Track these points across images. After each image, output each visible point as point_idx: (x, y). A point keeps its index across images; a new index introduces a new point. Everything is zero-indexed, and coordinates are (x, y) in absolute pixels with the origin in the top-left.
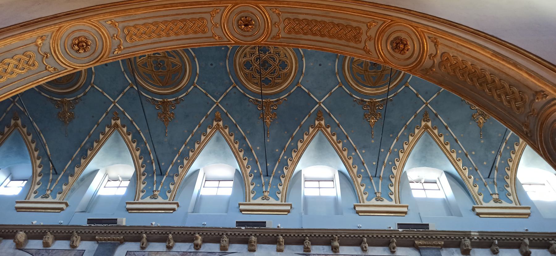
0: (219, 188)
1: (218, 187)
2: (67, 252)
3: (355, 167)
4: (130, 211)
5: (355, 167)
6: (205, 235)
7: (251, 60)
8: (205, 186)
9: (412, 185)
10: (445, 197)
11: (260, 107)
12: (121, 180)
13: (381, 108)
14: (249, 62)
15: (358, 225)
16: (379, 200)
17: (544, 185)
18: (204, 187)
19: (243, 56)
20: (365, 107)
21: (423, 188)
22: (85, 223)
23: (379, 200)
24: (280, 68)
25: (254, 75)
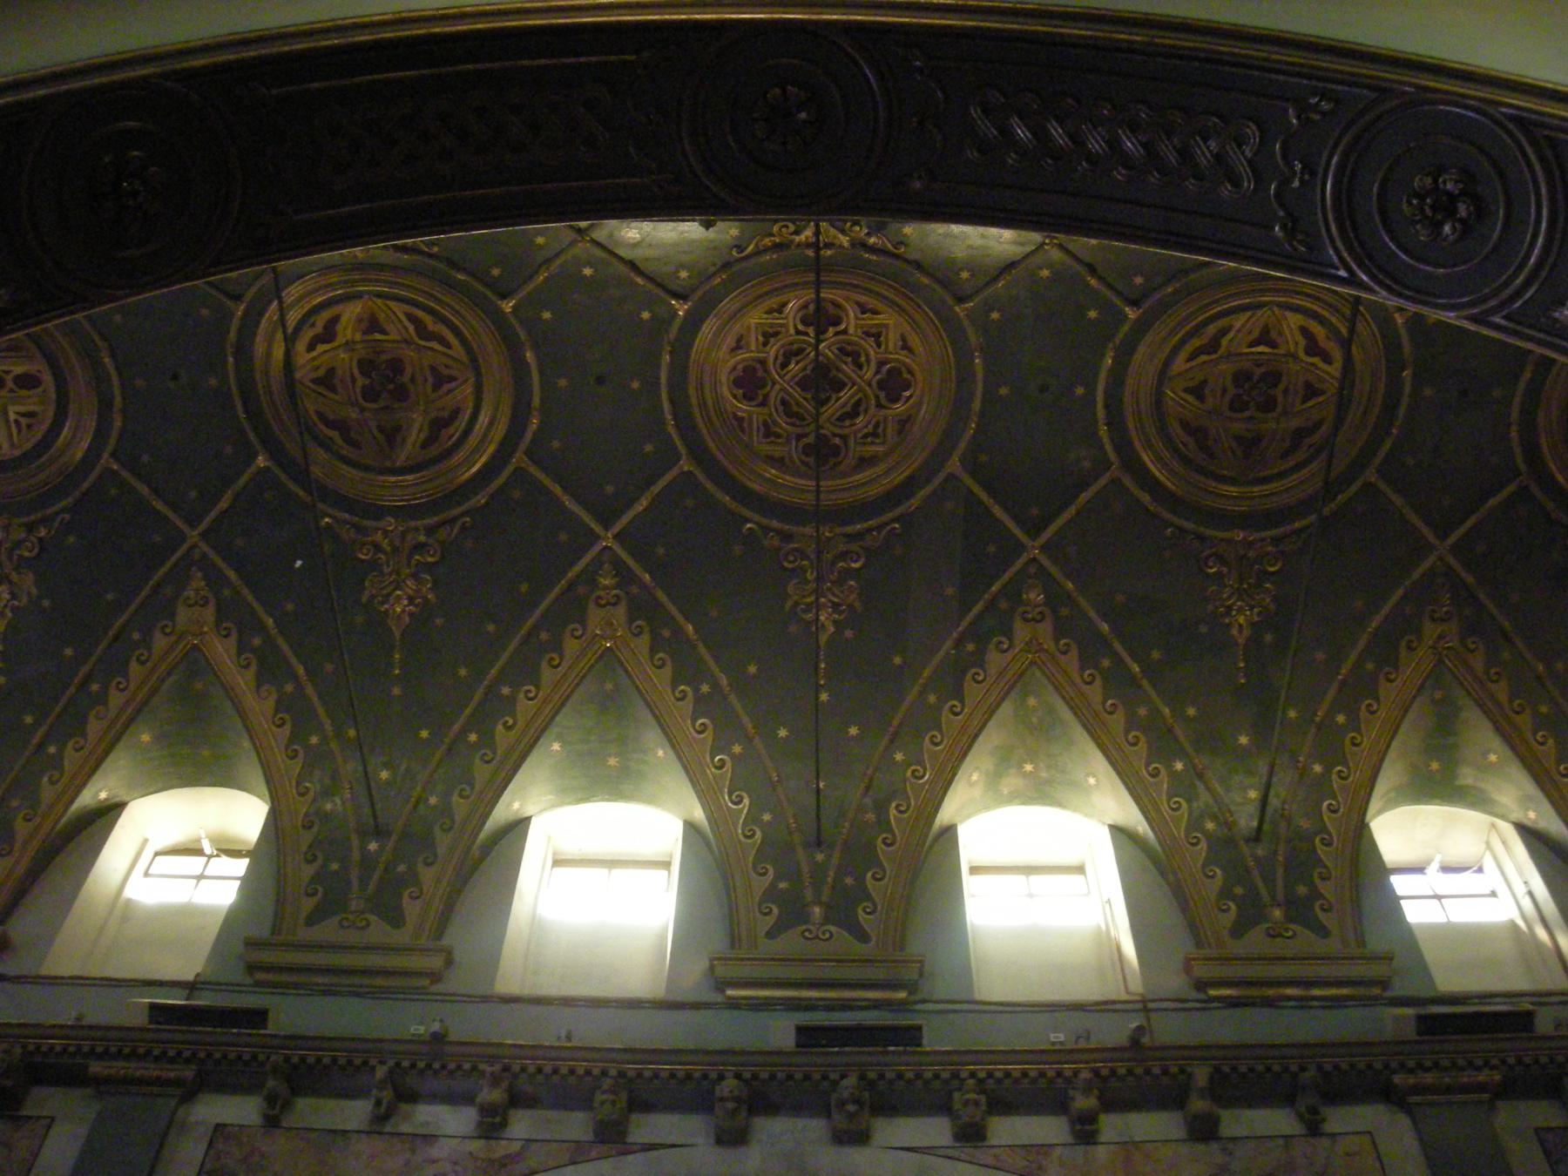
0: (203, 882)
1: (200, 877)
2: (363, 1136)
3: (1177, 805)
4: (261, 976)
5: (1177, 805)
6: (1511, 1067)
7: (763, 362)
8: (150, 872)
9: (1399, 883)
10: (1104, 927)
11: (792, 558)
12: (208, 850)
13: (1272, 569)
14: (755, 370)
15: (1052, 1035)
16: (817, 937)
17: (1080, 869)
18: (146, 874)
19: (730, 341)
20: (1211, 564)
21: (1443, 900)
22: (141, 1019)
23: (817, 937)
24: (877, 397)
25: (865, 431)
